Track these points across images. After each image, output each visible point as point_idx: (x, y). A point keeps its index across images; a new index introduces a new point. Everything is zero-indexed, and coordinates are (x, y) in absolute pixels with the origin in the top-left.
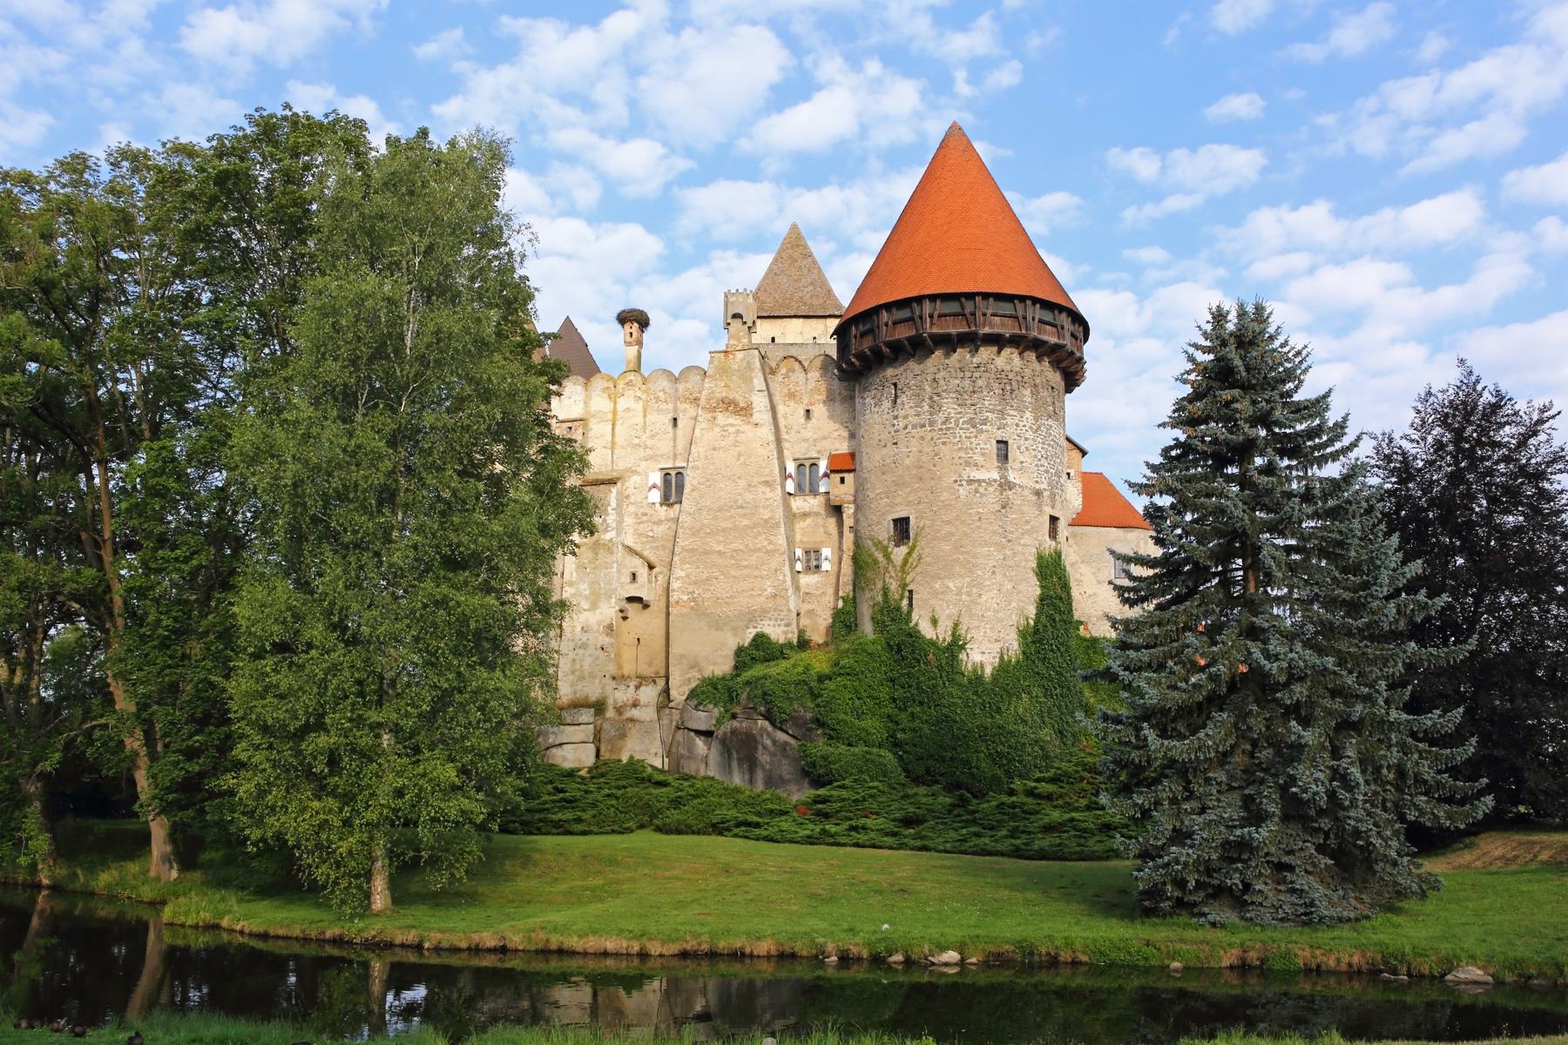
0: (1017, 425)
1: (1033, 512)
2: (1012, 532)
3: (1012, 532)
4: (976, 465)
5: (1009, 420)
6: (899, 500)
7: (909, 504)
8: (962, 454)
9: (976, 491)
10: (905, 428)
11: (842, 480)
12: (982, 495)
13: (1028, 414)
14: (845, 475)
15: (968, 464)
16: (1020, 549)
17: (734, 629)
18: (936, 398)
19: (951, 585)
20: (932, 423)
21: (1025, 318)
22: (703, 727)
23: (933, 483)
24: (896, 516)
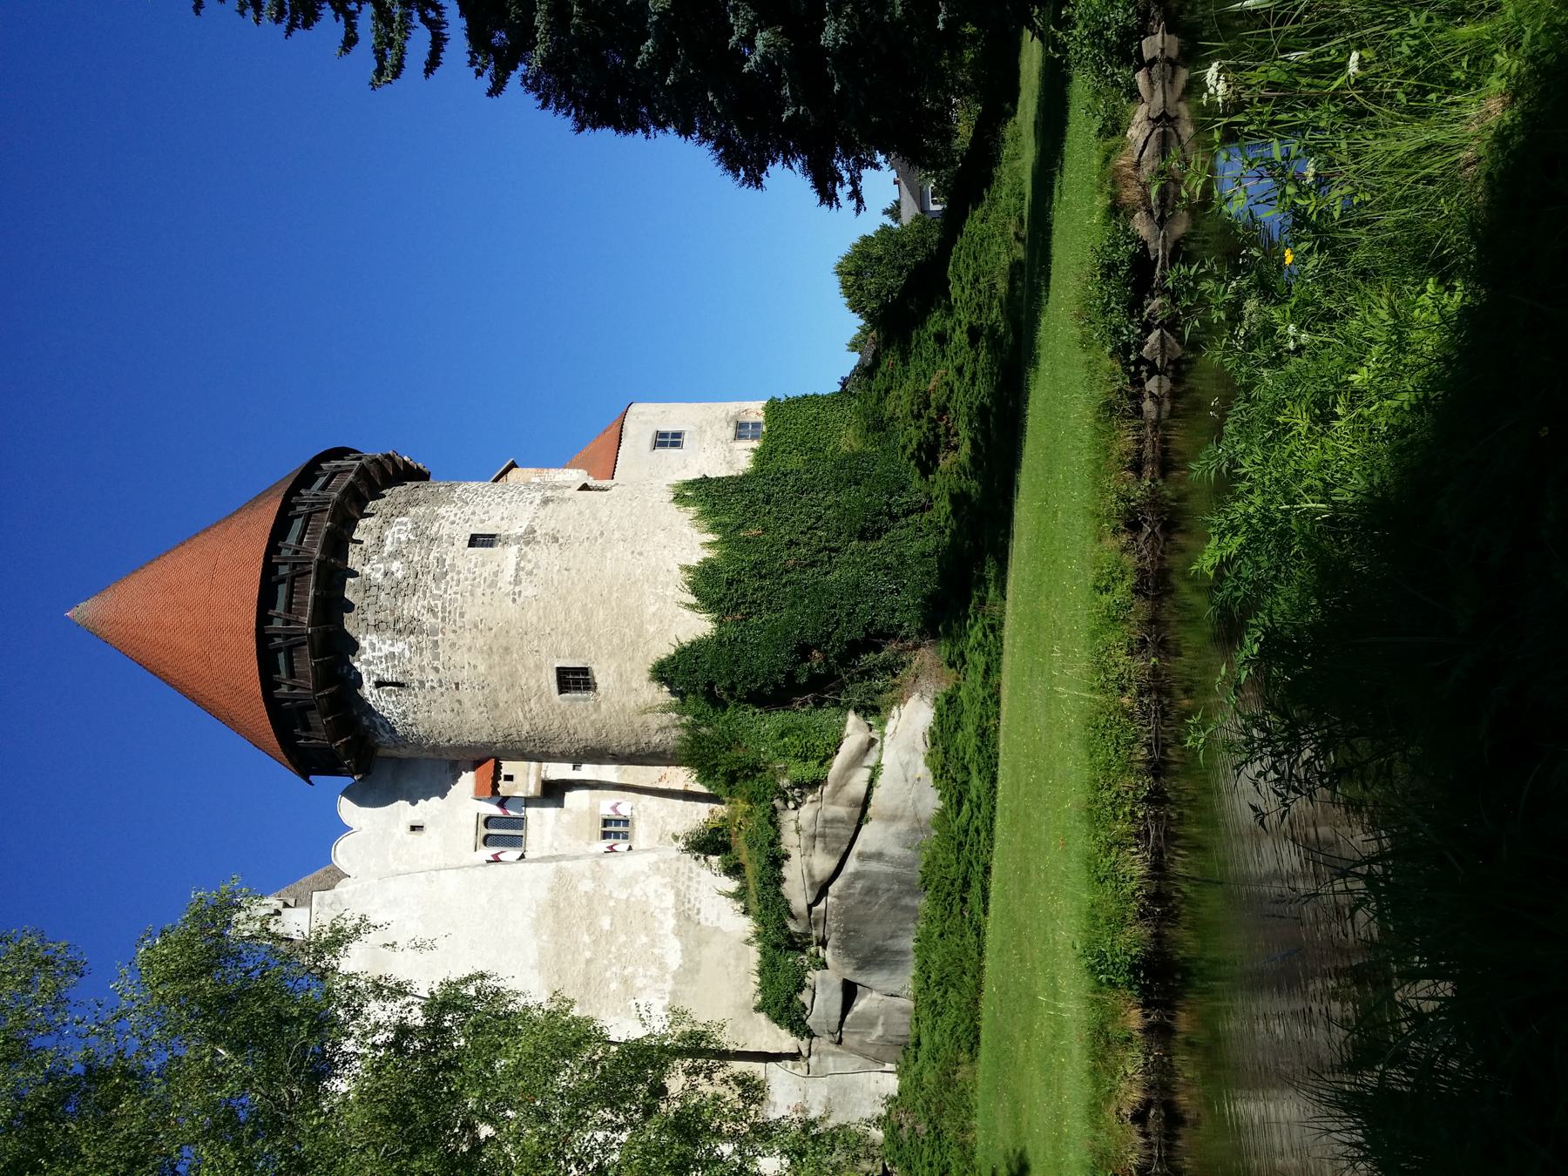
0: (453, 523)
1: (569, 508)
2: (591, 531)
3: (591, 531)
4: (496, 574)
5: (444, 532)
6: (532, 683)
7: (538, 667)
8: (479, 591)
9: (530, 573)
10: (436, 670)
11: (509, 778)
12: (537, 566)
13: (442, 511)
14: (504, 772)
15: (493, 584)
16: (613, 522)
17: (699, 945)
18: (401, 625)
19: (652, 609)
20: (434, 632)
21: (313, 505)
22: (838, 997)
23: (513, 632)
24: (554, 686)
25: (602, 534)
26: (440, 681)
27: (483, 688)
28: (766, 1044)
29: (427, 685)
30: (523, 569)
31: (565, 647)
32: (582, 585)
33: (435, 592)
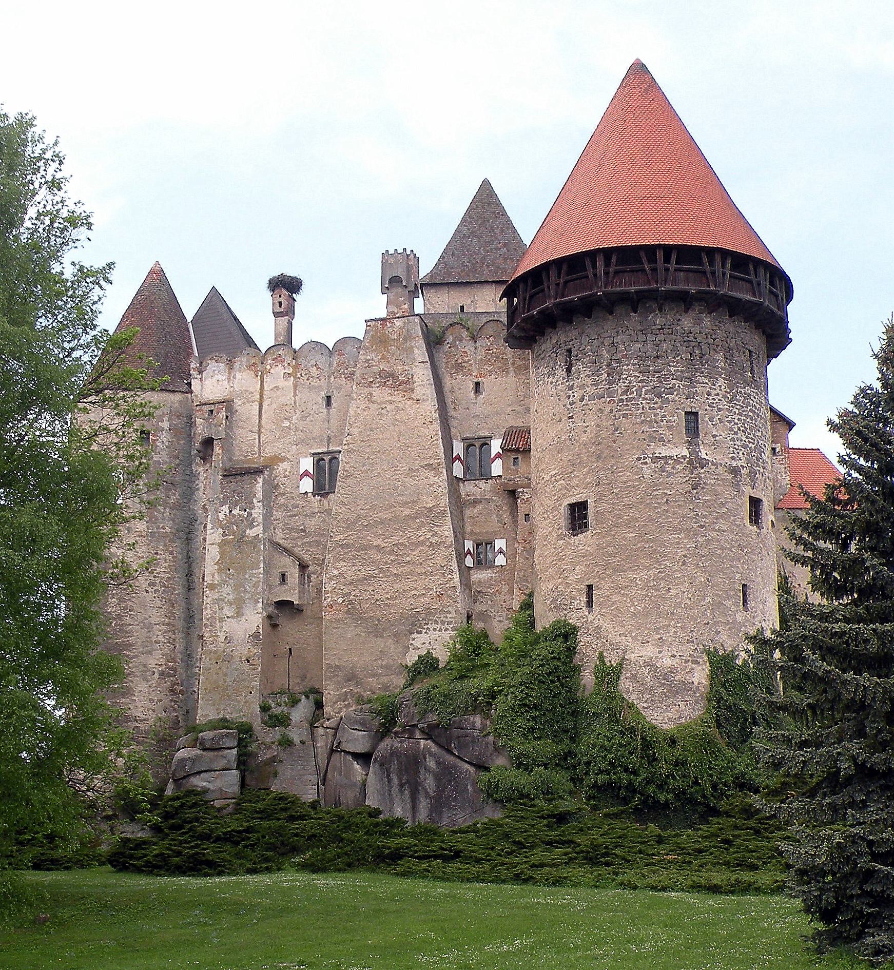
2: (705, 517)
4: (661, 440)
8: (646, 428)
10: (582, 400)
12: (669, 475)
13: (721, 382)
15: (652, 439)
24: (573, 500)
25: (702, 527)
26: (574, 403)
27: (571, 440)
28: (329, 693)
29: (571, 392)
30: (666, 463)
31: (603, 506)
32: (654, 516)
33: (643, 390)
